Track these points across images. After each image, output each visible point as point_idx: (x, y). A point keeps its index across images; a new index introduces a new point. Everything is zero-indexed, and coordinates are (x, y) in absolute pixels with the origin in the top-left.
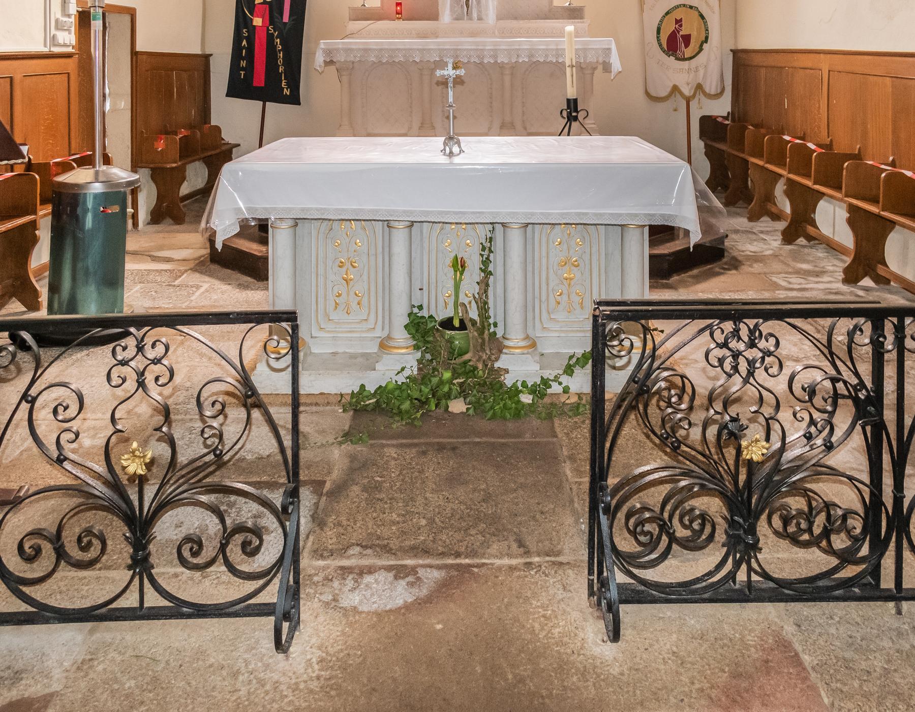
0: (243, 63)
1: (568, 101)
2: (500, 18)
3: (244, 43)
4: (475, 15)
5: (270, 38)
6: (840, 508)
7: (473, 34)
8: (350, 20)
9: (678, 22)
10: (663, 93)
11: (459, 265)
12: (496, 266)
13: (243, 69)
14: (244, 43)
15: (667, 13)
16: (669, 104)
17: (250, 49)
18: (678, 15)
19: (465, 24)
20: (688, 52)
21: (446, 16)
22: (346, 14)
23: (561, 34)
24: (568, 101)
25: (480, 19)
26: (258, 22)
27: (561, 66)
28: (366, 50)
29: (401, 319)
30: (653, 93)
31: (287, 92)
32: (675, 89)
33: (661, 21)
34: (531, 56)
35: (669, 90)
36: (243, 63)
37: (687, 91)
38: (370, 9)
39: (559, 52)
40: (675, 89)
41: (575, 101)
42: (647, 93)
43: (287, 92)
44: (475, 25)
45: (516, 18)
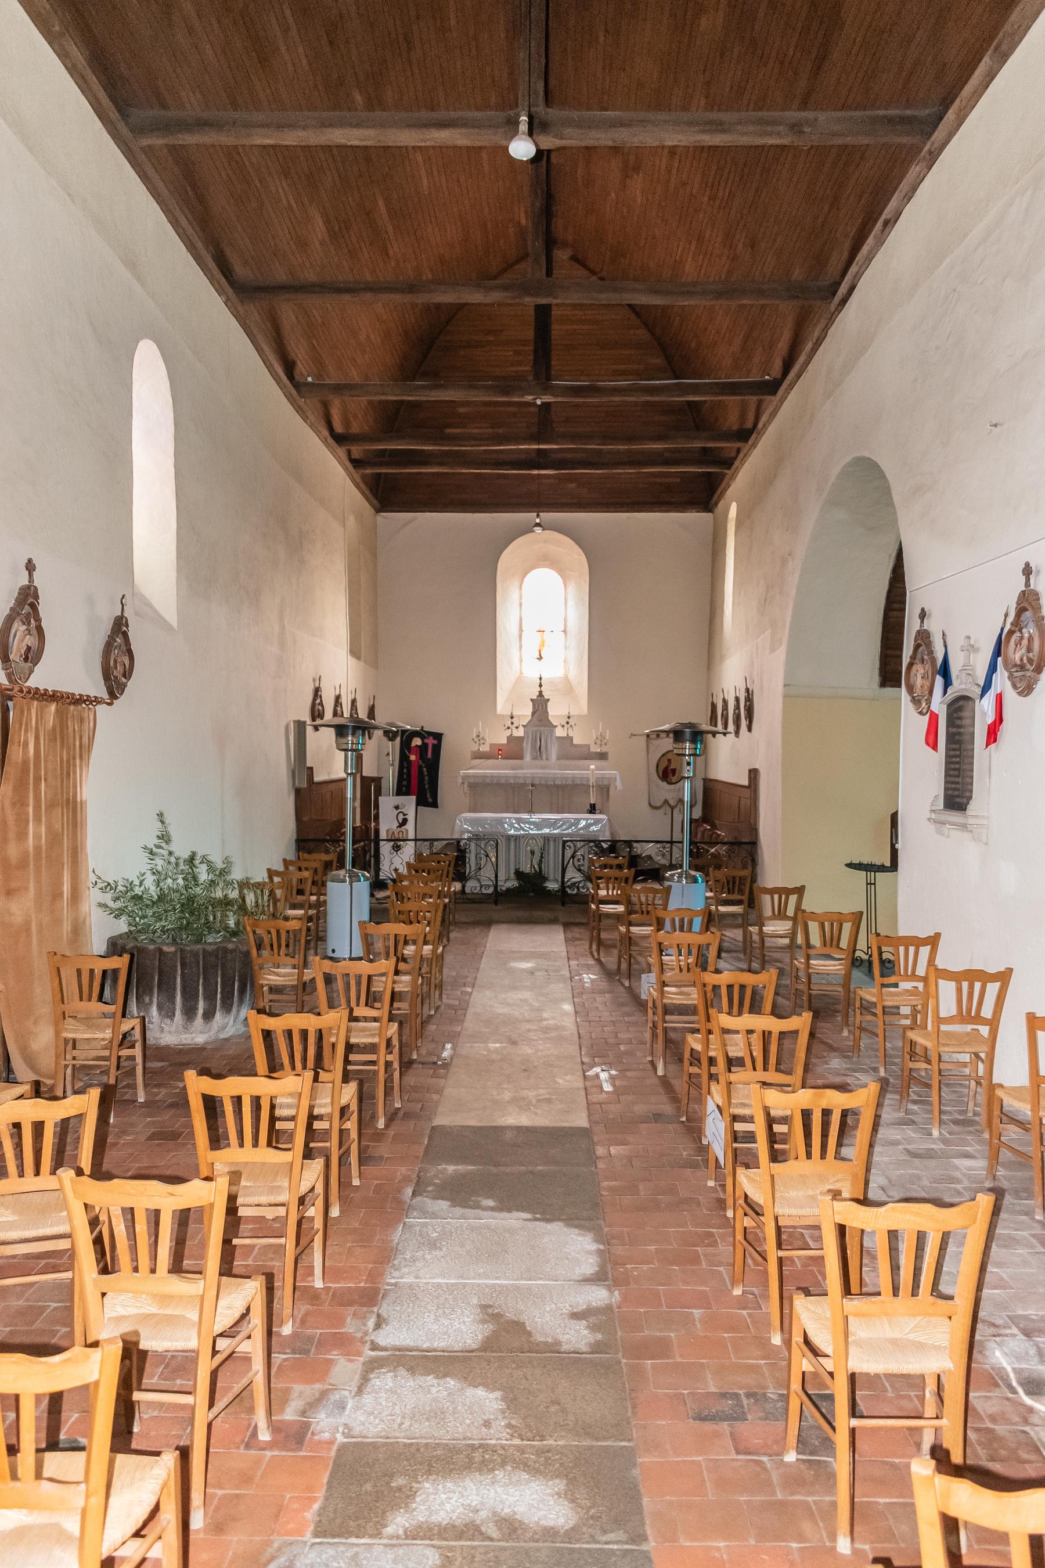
0: (405, 783)
1: (591, 805)
2: (559, 758)
3: (405, 770)
4: (544, 757)
5: (420, 767)
6: (737, 1032)
7: (543, 768)
8: (472, 758)
9: (669, 761)
10: (658, 804)
11: (533, 853)
12: (545, 855)
13: (405, 786)
14: (405, 770)
15: (663, 755)
16: (661, 811)
17: (409, 774)
18: (669, 756)
19: (538, 762)
20: (674, 779)
21: (528, 757)
22: (469, 756)
23: (588, 769)
24: (591, 805)
25: (547, 759)
26: (413, 758)
27: (589, 786)
28: (485, 777)
29: (512, 871)
30: (653, 804)
31: (430, 800)
32: (666, 802)
33: (659, 760)
34: (573, 781)
35: (662, 801)
36: (405, 783)
37: (672, 803)
38: (483, 752)
39: (588, 779)
40: (666, 802)
41: (594, 805)
42: (650, 804)
43: (430, 800)
44: (544, 762)
45: (568, 759)
